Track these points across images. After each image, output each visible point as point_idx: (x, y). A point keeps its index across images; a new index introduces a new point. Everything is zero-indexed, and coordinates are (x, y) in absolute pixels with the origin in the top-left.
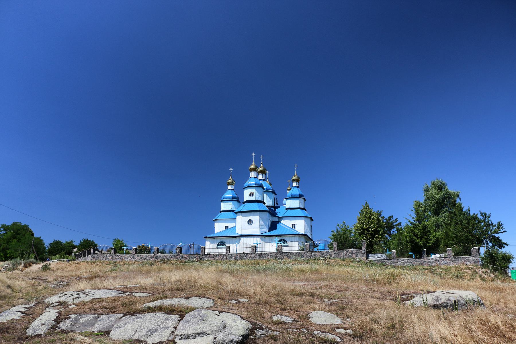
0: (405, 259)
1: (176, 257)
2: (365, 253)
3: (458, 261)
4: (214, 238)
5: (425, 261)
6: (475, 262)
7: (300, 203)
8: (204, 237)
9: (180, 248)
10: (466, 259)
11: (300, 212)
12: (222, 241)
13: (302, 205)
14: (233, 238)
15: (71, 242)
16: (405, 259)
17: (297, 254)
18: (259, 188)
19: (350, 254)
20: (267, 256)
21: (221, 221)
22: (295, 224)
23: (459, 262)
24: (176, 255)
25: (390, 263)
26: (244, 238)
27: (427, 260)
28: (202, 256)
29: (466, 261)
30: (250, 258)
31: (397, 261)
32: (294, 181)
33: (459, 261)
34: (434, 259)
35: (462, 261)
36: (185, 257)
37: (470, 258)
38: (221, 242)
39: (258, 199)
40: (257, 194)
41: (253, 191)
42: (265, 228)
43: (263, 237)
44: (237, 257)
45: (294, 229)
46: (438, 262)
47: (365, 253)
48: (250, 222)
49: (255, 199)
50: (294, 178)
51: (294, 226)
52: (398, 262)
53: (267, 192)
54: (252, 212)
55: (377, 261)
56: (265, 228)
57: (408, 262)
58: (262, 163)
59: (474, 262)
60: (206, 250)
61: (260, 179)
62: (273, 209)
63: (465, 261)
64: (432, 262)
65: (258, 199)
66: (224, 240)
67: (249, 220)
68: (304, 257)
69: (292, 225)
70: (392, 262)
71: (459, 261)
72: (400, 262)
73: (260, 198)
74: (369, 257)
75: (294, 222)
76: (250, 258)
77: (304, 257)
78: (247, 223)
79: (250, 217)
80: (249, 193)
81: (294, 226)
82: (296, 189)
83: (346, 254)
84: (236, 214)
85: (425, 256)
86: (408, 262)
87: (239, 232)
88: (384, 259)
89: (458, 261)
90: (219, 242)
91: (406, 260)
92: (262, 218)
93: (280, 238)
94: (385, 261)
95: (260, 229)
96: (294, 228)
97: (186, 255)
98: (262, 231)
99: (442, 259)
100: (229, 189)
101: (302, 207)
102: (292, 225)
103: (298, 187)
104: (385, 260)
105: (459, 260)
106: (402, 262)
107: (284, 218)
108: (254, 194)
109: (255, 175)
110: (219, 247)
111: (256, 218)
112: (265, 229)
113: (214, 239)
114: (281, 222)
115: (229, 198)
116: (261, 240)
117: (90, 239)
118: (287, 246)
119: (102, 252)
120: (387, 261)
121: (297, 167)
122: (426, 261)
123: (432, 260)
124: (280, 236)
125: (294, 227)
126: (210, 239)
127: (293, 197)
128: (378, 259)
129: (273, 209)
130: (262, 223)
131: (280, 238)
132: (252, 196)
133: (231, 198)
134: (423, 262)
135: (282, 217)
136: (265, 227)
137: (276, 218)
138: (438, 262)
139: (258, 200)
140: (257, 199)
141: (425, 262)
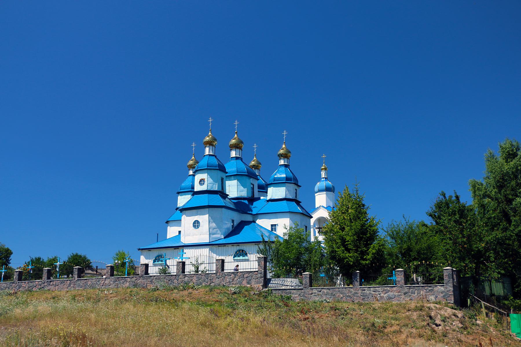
0: (323, 288)
1: (13, 286)
2: (261, 277)
3: (415, 294)
4: (149, 249)
5: (357, 293)
6: (444, 296)
7: (287, 191)
8: (139, 249)
9: (18, 272)
10: (429, 290)
11: (284, 206)
12: (160, 254)
13: (290, 193)
14: (175, 249)
15: (55, 258)
16: (323, 288)
17: (164, 278)
18: (212, 170)
19: (239, 278)
20: (125, 283)
21: (174, 223)
22: (276, 225)
23: (416, 295)
24: (13, 283)
25: (299, 295)
26: (188, 249)
27: (360, 291)
28: (44, 284)
29: (428, 294)
30: (103, 285)
31: (310, 292)
32: (281, 156)
33: (416, 293)
34: (371, 288)
35: (421, 293)
36: (23, 285)
37: (436, 289)
38: (158, 256)
39: (212, 188)
40: (211, 180)
41: (204, 176)
42: (218, 233)
43: (214, 247)
44: (87, 284)
45: (274, 232)
46: (379, 294)
47: (261, 277)
48: (196, 224)
49: (206, 189)
50: (281, 152)
51: (274, 226)
52: (312, 294)
53: (237, 176)
54: (199, 209)
55: (280, 291)
56: (218, 233)
57: (327, 294)
58: (236, 133)
59: (442, 295)
60: (226, 265)
61: (233, 156)
62: (246, 202)
63: (427, 294)
64: (369, 295)
65: (212, 188)
66: (163, 252)
67: (196, 221)
68: (174, 283)
69: (272, 225)
70: (302, 294)
71: (416, 293)
72: (315, 293)
73: (216, 186)
74: (270, 285)
75: (274, 221)
76: (103, 285)
77: (174, 283)
78: (192, 226)
79: (197, 216)
80: (199, 180)
81: (274, 226)
82: (283, 168)
83: (233, 280)
84: (181, 212)
85: (357, 284)
86: (327, 294)
87: (185, 240)
88: (293, 288)
89: (415, 294)
90: (156, 255)
91: (325, 291)
92: (212, 219)
93: (238, 248)
94: (292, 291)
95: (210, 234)
96: (275, 231)
97: (24, 283)
98: (213, 238)
99: (385, 290)
100: (190, 175)
101: (291, 197)
102: (272, 225)
103: (286, 166)
104: (291, 291)
105: (416, 291)
106: (318, 295)
107: (260, 216)
108: (206, 180)
109: (211, 151)
110: (156, 263)
111: (204, 219)
112: (218, 234)
113: (150, 251)
114: (256, 222)
115: (188, 189)
116: (211, 252)
117: (81, 253)
118: (248, 260)
119: (97, 272)
120: (295, 291)
121: (212, 121)
122: (358, 292)
123: (368, 291)
124: (238, 245)
125: (275, 228)
126: (145, 252)
127: (277, 183)
128: (284, 288)
129: (246, 202)
130: (214, 225)
131: (238, 248)
132: (203, 184)
133: (190, 189)
134: (353, 294)
135: (257, 214)
136: (219, 232)
137: (249, 216)
138: (379, 294)
139: (212, 189)
140: (209, 189)
141: (356, 295)
